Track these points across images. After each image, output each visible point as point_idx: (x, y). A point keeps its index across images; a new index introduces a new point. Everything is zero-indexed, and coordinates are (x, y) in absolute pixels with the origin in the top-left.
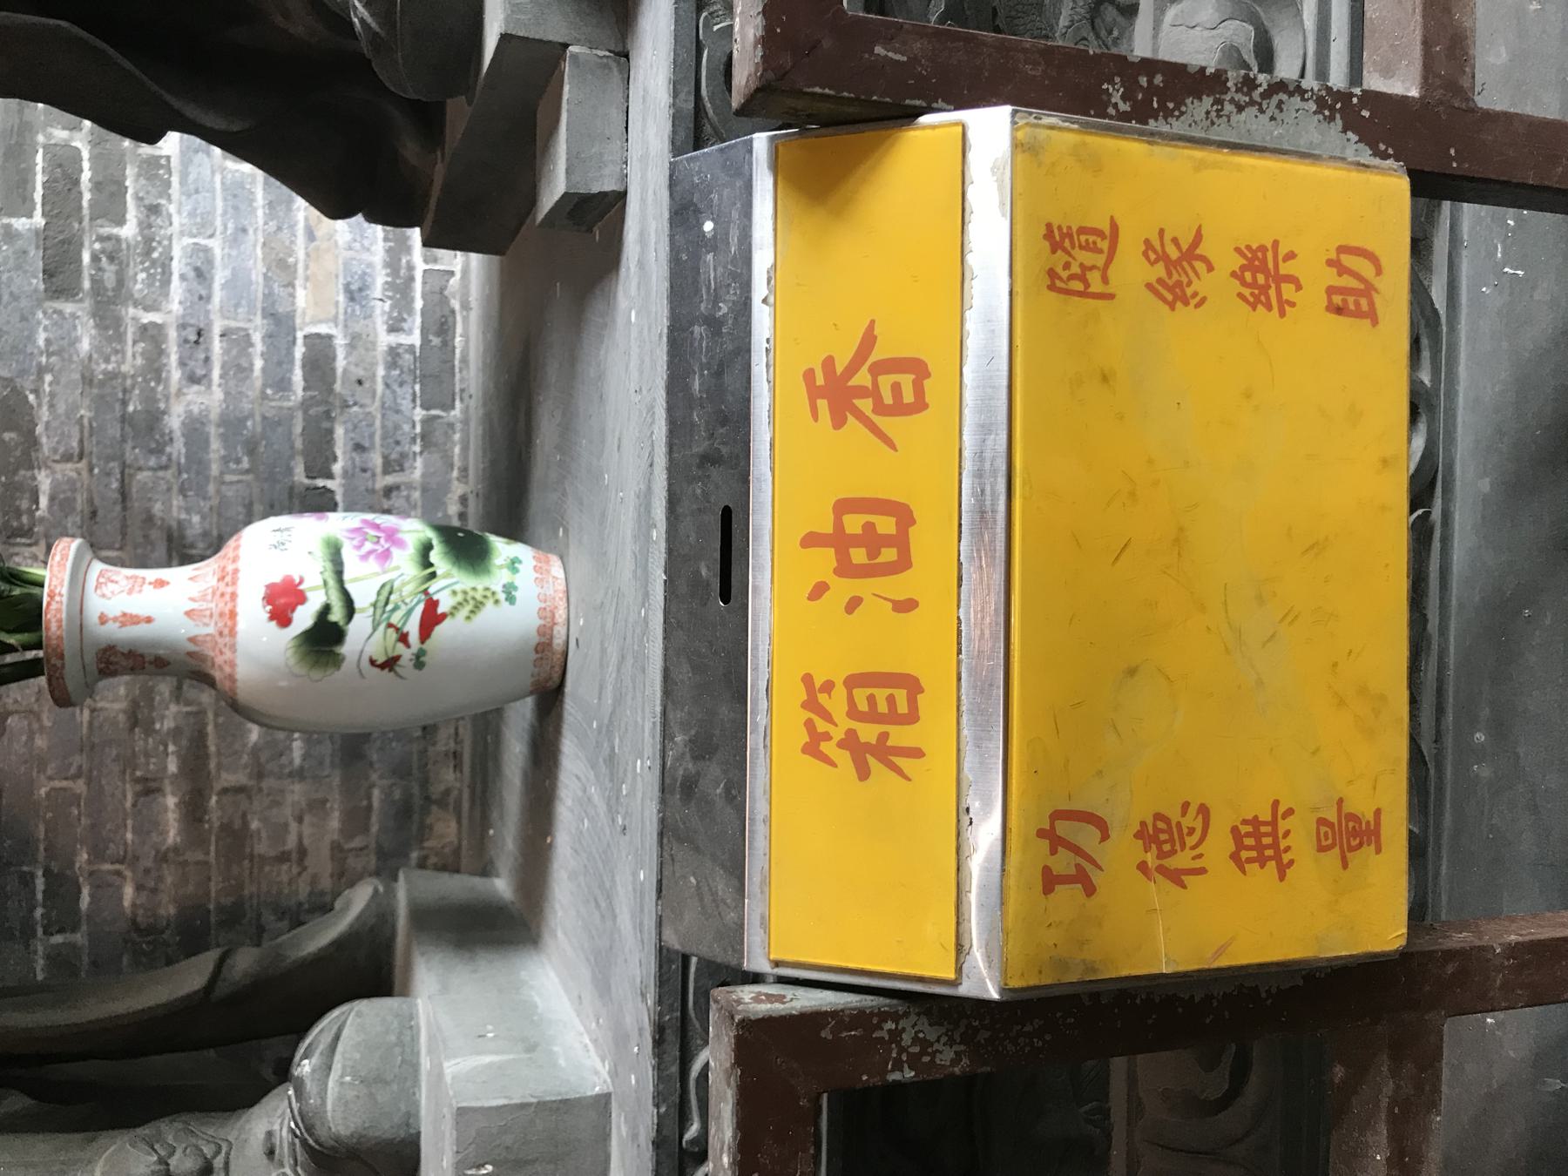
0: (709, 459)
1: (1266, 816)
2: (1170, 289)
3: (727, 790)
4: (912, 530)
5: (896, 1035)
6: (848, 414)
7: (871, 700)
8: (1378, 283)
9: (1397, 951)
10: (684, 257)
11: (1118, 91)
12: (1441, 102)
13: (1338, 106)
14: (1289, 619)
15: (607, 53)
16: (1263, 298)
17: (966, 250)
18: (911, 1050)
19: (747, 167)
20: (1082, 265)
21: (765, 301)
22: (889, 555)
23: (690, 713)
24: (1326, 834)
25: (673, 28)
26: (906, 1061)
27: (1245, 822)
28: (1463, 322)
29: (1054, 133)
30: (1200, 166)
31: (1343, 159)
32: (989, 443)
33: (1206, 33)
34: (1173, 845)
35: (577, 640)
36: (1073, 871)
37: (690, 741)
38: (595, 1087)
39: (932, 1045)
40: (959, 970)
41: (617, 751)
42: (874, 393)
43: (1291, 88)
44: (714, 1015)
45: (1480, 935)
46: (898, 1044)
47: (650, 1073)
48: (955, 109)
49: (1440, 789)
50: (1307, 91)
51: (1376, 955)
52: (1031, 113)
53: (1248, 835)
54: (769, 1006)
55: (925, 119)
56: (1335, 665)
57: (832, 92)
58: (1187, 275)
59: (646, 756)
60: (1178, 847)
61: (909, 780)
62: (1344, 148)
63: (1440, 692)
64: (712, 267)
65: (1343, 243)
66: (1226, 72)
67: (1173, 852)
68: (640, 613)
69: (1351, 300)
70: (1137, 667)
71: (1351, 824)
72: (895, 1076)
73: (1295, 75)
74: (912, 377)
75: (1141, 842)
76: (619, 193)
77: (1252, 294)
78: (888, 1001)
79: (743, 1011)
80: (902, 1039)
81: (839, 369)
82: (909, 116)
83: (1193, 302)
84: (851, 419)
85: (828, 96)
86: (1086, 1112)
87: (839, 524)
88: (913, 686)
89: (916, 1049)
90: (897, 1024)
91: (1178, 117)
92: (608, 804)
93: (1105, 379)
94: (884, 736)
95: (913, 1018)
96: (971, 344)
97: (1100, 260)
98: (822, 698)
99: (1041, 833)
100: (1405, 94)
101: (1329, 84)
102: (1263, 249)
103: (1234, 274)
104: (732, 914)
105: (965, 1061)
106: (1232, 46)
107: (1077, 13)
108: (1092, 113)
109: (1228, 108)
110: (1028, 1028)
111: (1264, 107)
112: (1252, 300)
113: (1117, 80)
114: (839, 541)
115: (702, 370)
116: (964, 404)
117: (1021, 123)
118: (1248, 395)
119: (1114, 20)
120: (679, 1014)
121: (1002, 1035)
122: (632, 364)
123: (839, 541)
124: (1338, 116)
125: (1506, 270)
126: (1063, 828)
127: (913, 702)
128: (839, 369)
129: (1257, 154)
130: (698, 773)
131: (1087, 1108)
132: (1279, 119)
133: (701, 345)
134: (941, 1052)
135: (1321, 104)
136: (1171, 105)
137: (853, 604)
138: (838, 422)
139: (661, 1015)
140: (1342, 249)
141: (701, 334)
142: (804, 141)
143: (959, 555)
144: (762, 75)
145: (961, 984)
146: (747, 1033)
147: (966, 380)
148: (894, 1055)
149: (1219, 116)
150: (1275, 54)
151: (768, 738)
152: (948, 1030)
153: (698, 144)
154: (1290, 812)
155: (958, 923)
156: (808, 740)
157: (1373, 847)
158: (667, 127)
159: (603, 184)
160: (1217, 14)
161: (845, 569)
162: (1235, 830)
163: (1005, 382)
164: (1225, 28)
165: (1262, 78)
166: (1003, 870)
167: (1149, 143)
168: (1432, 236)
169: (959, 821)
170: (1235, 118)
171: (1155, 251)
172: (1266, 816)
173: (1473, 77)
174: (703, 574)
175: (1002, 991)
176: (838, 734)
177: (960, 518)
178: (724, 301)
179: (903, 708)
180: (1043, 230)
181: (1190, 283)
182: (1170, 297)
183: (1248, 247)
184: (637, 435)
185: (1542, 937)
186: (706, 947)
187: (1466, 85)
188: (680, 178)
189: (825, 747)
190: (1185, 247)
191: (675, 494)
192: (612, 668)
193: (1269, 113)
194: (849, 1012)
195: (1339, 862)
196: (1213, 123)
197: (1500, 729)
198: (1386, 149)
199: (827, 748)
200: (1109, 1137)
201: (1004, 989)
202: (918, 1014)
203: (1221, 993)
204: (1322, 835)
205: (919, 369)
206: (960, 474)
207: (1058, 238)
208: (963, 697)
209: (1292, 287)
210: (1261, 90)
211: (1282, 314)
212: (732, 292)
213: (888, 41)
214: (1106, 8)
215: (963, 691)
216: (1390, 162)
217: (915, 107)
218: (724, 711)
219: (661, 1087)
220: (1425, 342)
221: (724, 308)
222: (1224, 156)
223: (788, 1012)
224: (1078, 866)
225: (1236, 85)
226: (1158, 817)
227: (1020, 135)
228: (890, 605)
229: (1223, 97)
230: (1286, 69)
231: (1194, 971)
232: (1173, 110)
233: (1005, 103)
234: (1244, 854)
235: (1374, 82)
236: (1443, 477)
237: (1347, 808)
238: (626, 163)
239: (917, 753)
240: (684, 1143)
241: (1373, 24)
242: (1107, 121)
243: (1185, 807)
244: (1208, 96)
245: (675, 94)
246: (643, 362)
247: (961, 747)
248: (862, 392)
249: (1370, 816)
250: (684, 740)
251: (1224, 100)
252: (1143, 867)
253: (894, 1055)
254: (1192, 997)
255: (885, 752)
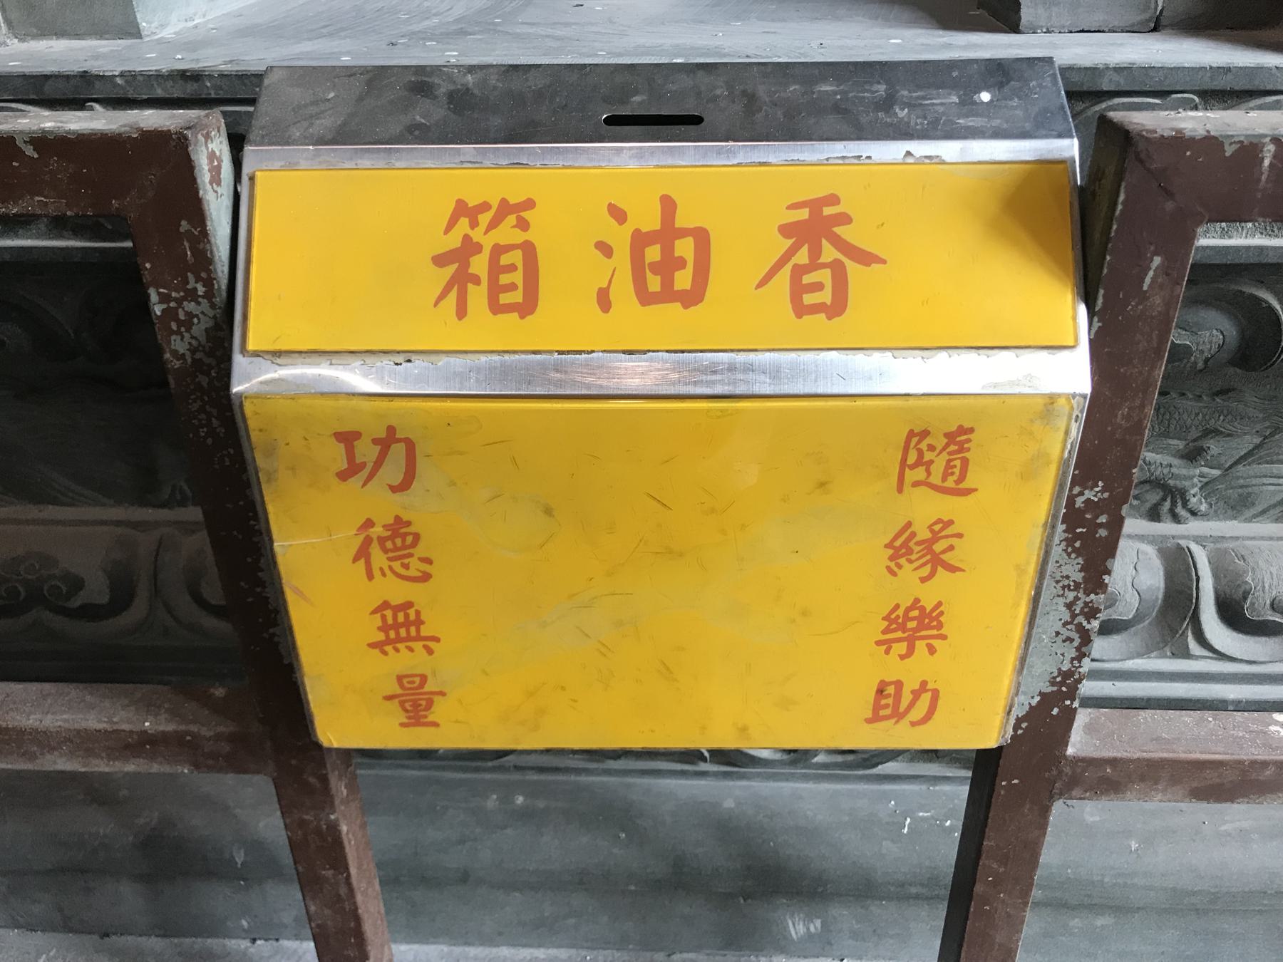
0: (751, 100)
1: (424, 631)
2: (905, 544)
3: (419, 126)
4: (678, 305)
5: (192, 295)
6: (793, 240)
7: (512, 268)
8: (905, 723)
9: (318, 739)
10: (955, 74)
11: (1095, 496)
12: (1060, 772)
13: (1064, 689)
14: (603, 650)
15: (1160, 8)
16: (894, 626)
17: (950, 351)
18: (180, 311)
19: (1044, 133)
20: (931, 462)
21: (909, 154)
22: (654, 283)
23: (495, 88)
24: (413, 682)
25: (1186, 65)
26: (169, 306)
27: (418, 613)
28: (866, 787)
29: (1061, 435)
30: (1020, 570)
31: (1017, 694)
32: (762, 377)
33: (1129, 580)
34: (392, 551)
35: (582, 5)
36: (358, 460)
37: (468, 89)
38: (147, 22)
39: (188, 330)
40: (256, 354)
41: (469, 37)
42: (814, 265)
43: (1084, 649)
44: (194, 114)
45: (346, 802)
46: (184, 299)
47: (154, 68)
48: (1090, 340)
49: (477, 770)
50: (1080, 662)
51: (312, 722)
52: (1082, 412)
53: (407, 616)
54: (206, 168)
55: (1082, 310)
56: (563, 688)
57: (1118, 212)
58: (917, 559)
59: (459, 58)
60: (391, 555)
61: (435, 306)
62: (1025, 693)
63: (556, 770)
64: (943, 101)
65: (941, 695)
66: (1104, 593)
67: (386, 551)
68: (601, 51)
69: (890, 701)
70: (554, 516)
71: (424, 703)
72: (154, 297)
73: (1095, 654)
74: (829, 302)
75: (391, 521)
76: (1018, 25)
77: (898, 617)
78: (224, 287)
79: (197, 141)
80: (189, 302)
81: (838, 230)
82: (1088, 297)
83: (892, 565)
84: (789, 243)
85: (1114, 210)
86: (181, 487)
87: (684, 233)
88: (527, 307)
89: (182, 316)
90: (203, 297)
91: (1065, 551)
92: (419, 32)
93: (822, 485)
94: (476, 280)
95: (211, 313)
96: (859, 357)
97: (936, 479)
98: (511, 219)
99: (391, 430)
100: (1070, 743)
101: (1084, 681)
102: (940, 626)
103: (917, 600)
104: (298, 134)
105: (177, 364)
106: (1116, 601)
107: (1156, 468)
108: (1076, 472)
109: (1071, 596)
110: (215, 422)
111: (1069, 627)
112: (893, 616)
113: (1106, 495)
114: (668, 232)
115: (841, 93)
116: (800, 353)
117: (1074, 402)
118: (805, 613)
119: (1147, 501)
120: (213, 96)
121: (206, 398)
122: (848, 41)
123: (668, 232)
124: (1055, 688)
125: (909, 820)
126: (398, 450)
127: (509, 308)
128: (838, 230)
129: (1028, 620)
130: (436, 97)
131: (185, 487)
132: (1057, 639)
133: (867, 91)
134: (182, 339)
135: (1067, 675)
136: (1077, 544)
137: (605, 249)
138: (785, 230)
139: (210, 77)
140: (936, 694)
141: (877, 92)
142: (1068, 190)
143: (654, 351)
144: (1143, 136)
145: (244, 356)
146: (174, 144)
147: (824, 354)
148: (174, 294)
149: (1063, 587)
150: (1104, 636)
151: (470, 165)
152: (204, 347)
153: (1070, 95)
154: (430, 651)
155: (300, 352)
156: (470, 205)
157: (405, 720)
158: (1087, 63)
159: (1028, 7)
160: (1145, 588)
161: (640, 241)
162: (409, 605)
163: (820, 391)
164: (1133, 595)
165: (1095, 624)
166: (354, 394)
167: (1046, 523)
168: (940, 762)
169: (398, 352)
170: (1061, 601)
171: (942, 530)
172: (424, 631)
173: (1081, 799)
174: (634, 98)
175: (240, 395)
176: (477, 235)
177: (690, 351)
178: (909, 114)
179: (505, 298)
180: (967, 425)
181: (910, 561)
182: (898, 543)
183: (942, 613)
184: (779, 46)
185: (348, 850)
186: (266, 111)
187: (1074, 793)
188: (1036, 68)
189: (464, 223)
190: (945, 557)
191: (716, 68)
192: (550, 31)
193: (1063, 631)
194: (209, 248)
195: (389, 693)
196: (1057, 582)
197: (525, 815)
198: (1021, 728)
199: (463, 224)
200: (163, 505)
201: (241, 397)
202: (215, 317)
203: (268, 595)
204: (411, 679)
205: (837, 307)
206: (732, 351)
207: (958, 439)
208: (517, 356)
209: (904, 652)
210: (1085, 623)
211: (879, 643)
212: (918, 121)
213: (1165, 270)
214: (1158, 494)
215: (523, 356)
216: (1010, 732)
217: (1095, 299)
218: (496, 121)
219: (141, 78)
220: (850, 758)
221: (903, 113)
222: (1028, 590)
223: (201, 186)
224: (364, 465)
225: (1091, 601)
226: (417, 537)
227: (1062, 401)
228: (605, 285)
229: (1081, 591)
230: (1100, 646)
231: (278, 570)
232: (1073, 547)
233: (1093, 388)
234: (389, 613)
235: (1083, 717)
236: (737, 772)
237: (436, 699)
238: (1048, 32)
239: (461, 312)
240: (89, 104)
241: (1133, 717)
242: (1069, 486)
243: (428, 561)
244: (1084, 577)
245: (1118, 70)
246: (851, 49)
247: (469, 355)
248: (815, 252)
249: (431, 718)
250: (468, 82)
251: (1079, 592)
252: (369, 524)
253: (174, 294)
254: (262, 570)
255: (462, 280)
